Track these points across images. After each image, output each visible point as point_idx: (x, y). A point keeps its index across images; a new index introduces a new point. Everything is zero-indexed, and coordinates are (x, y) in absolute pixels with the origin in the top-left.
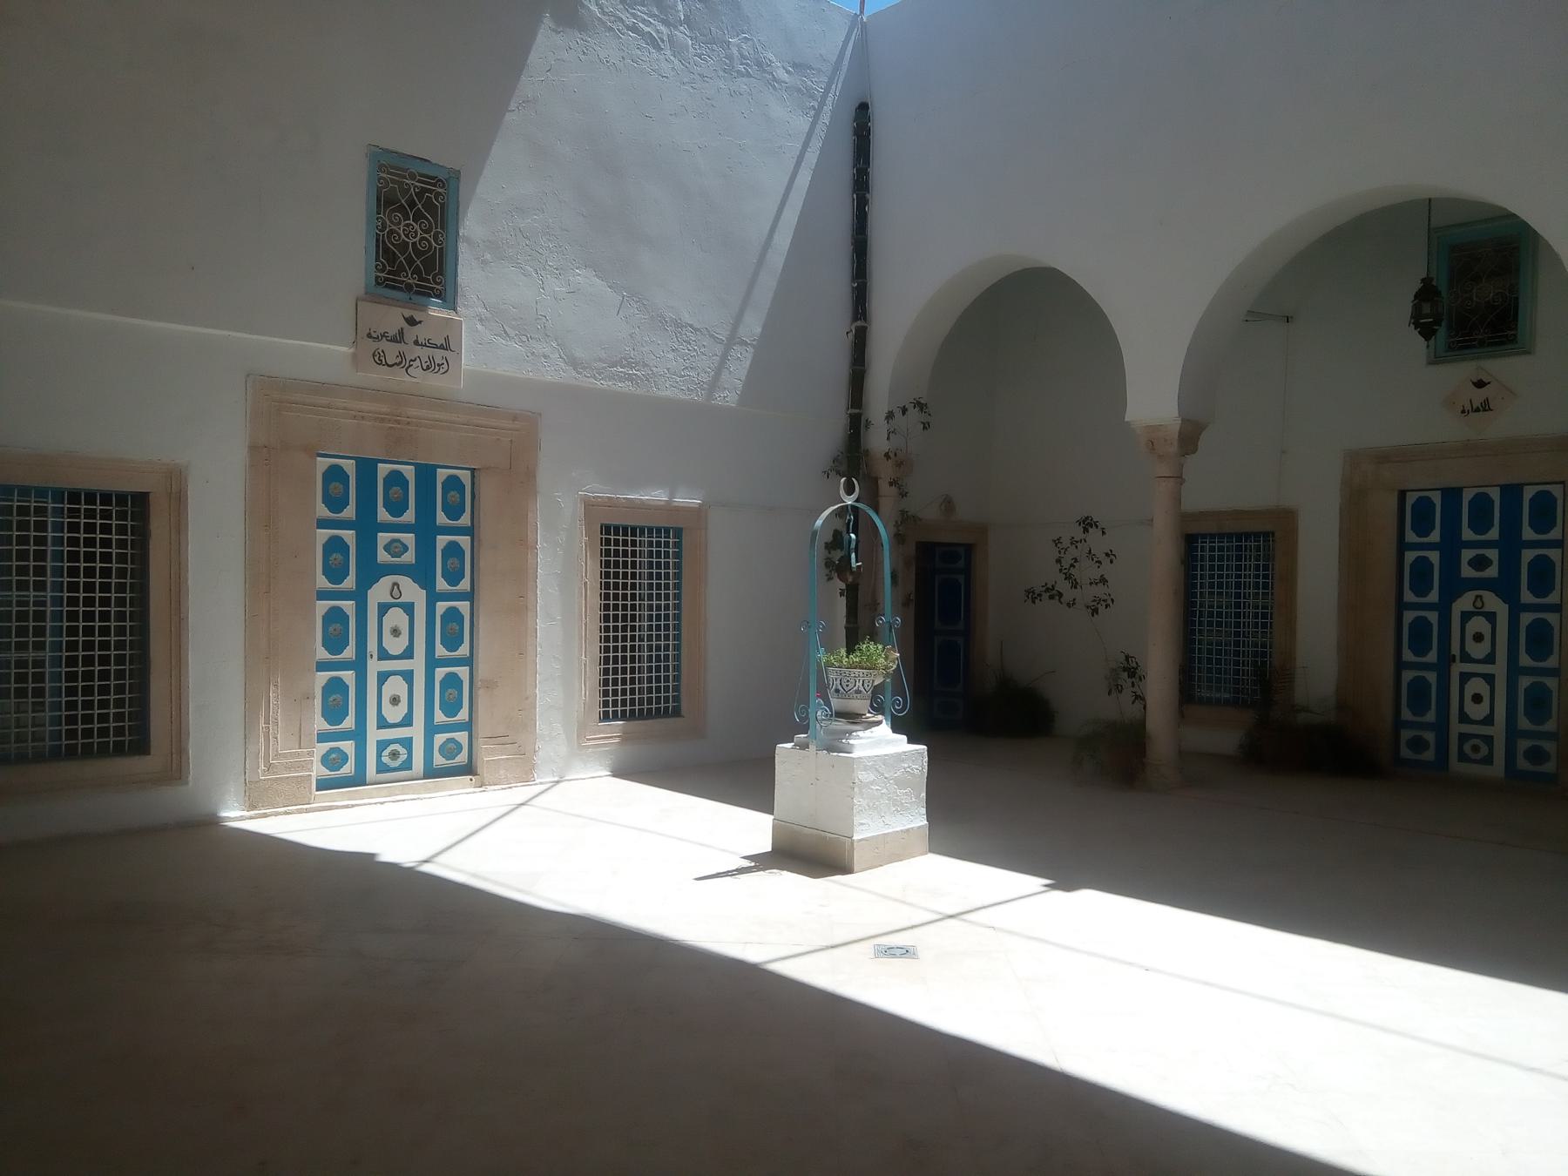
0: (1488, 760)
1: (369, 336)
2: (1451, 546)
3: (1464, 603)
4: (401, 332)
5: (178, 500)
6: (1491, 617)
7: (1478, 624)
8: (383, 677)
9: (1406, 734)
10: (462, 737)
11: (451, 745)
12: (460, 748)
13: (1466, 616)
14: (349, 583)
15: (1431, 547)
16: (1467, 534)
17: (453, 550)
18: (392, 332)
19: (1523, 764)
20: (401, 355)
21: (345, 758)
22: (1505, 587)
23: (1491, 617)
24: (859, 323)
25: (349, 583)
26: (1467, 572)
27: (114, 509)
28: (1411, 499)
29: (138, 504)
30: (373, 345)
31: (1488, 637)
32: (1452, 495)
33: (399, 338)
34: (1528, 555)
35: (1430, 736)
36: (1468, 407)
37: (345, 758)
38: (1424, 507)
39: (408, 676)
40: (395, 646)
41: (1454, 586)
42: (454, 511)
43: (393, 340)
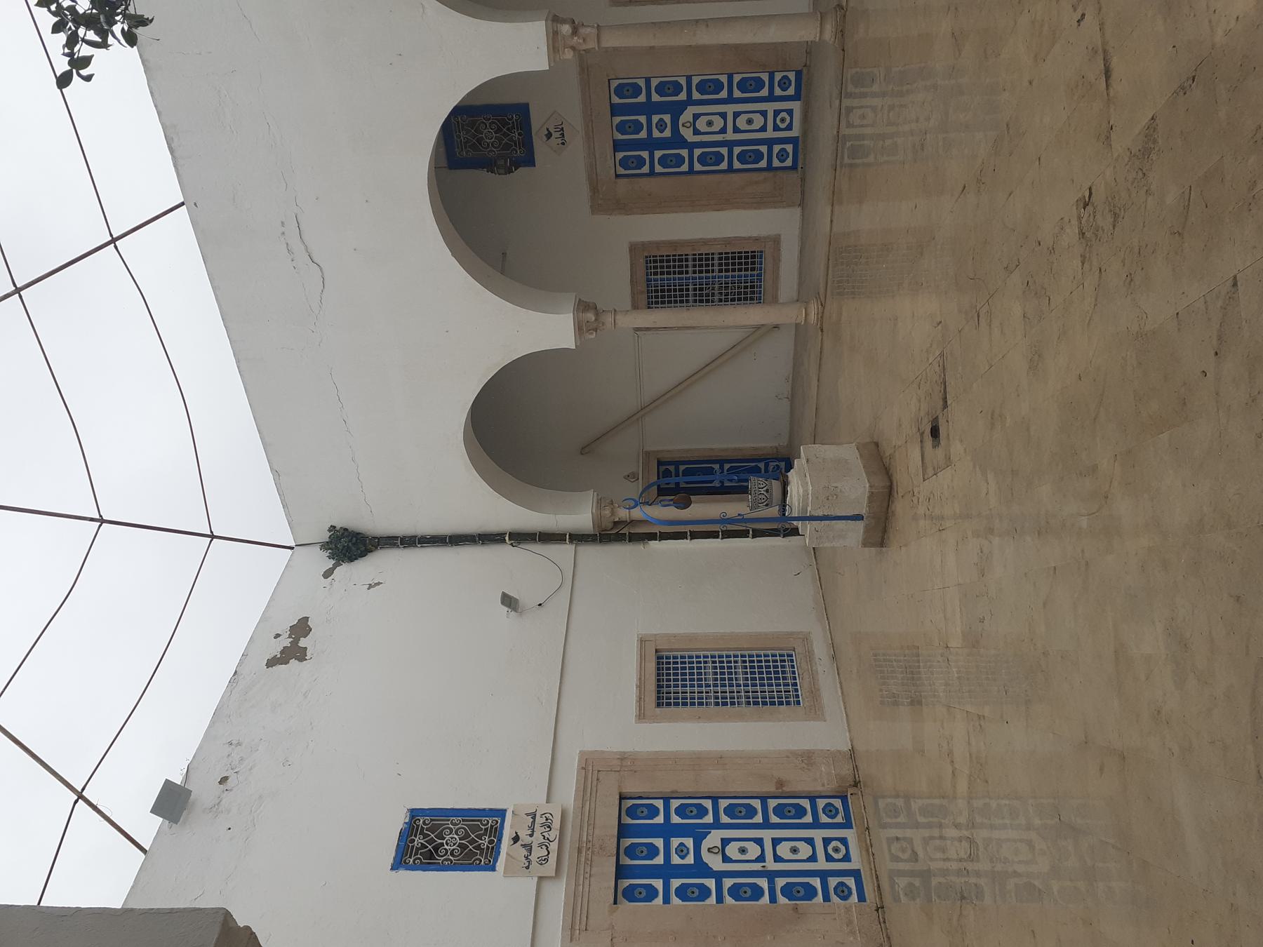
0: (790, 112)
1: (527, 868)
2: (651, 144)
4: (524, 846)
6: (696, 117)
7: (701, 125)
8: (777, 859)
9: (776, 163)
10: (821, 803)
11: (846, 892)
12: (829, 804)
13: (696, 132)
14: (711, 883)
15: (649, 95)
16: (643, 134)
18: (524, 852)
19: (791, 91)
20: (541, 845)
21: (782, 161)
22: (676, 110)
23: (696, 117)
25: (711, 883)
26: (667, 133)
27: (665, 690)
28: (621, 171)
29: (662, 700)
30: (534, 864)
31: (710, 118)
32: (617, 146)
33: (529, 847)
34: (656, 98)
35: (777, 148)
36: (560, 141)
37: (784, 90)
38: (624, 163)
41: (677, 141)
42: (636, 91)
43: (530, 851)
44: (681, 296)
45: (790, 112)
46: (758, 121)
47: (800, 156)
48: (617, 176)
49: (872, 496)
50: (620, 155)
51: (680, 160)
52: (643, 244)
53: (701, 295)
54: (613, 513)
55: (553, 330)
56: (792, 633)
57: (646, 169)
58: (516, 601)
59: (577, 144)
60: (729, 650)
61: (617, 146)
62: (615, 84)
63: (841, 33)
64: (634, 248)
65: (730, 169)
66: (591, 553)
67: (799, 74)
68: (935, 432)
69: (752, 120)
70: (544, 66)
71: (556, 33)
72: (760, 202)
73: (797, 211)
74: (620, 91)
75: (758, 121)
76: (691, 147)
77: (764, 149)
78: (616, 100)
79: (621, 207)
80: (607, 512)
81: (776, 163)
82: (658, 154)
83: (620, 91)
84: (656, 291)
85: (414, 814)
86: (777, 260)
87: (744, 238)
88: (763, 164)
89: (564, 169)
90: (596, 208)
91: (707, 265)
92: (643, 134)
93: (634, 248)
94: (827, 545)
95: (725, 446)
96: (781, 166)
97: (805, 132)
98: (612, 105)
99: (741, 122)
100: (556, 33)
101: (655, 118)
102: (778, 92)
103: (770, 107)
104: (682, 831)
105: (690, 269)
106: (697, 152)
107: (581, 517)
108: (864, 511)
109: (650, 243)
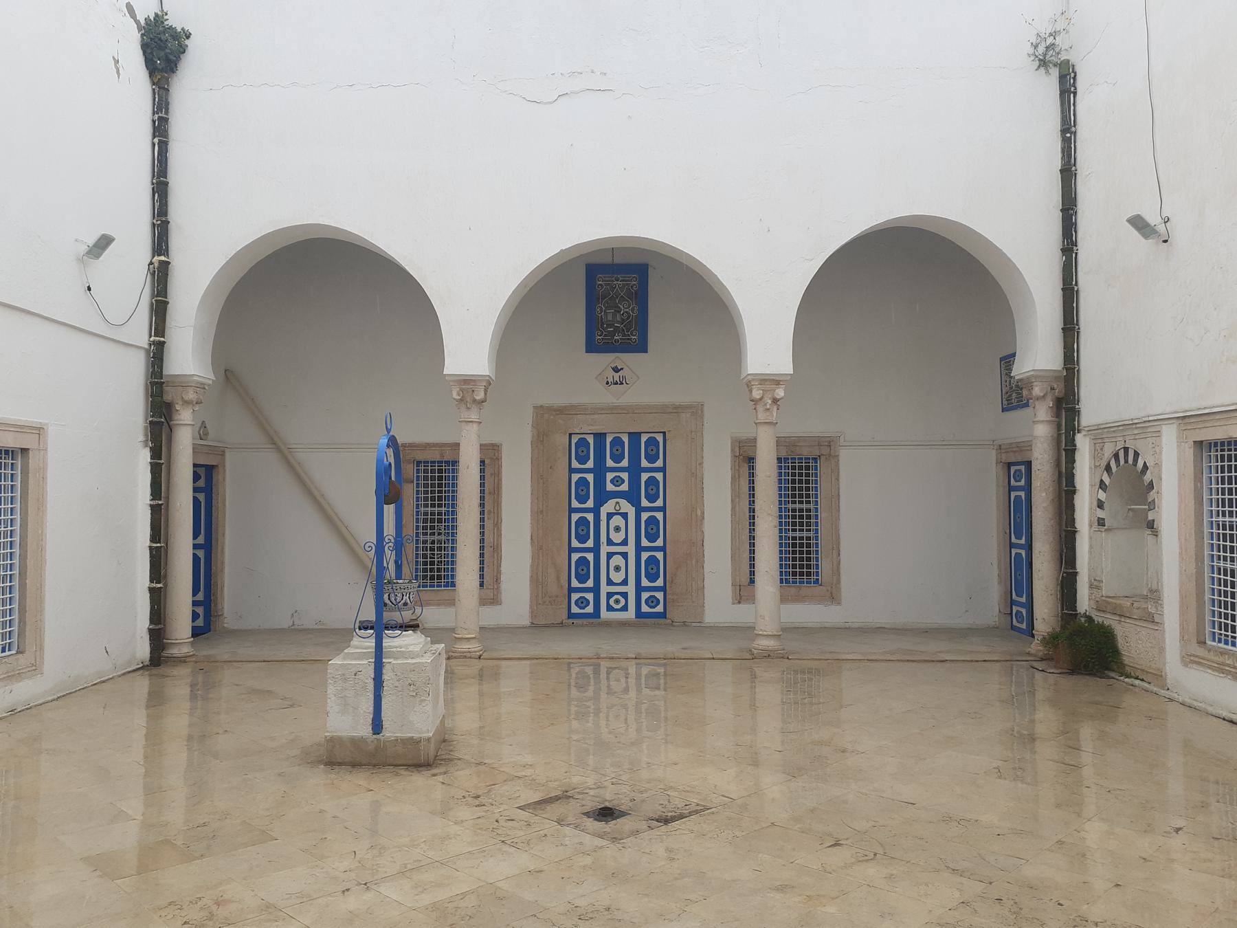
0: (625, 608)
2: (600, 471)
6: (625, 516)
7: (617, 521)
13: (610, 516)
15: (613, 470)
16: (610, 463)
17: (652, 482)
19: (645, 608)
21: (658, 602)
23: (625, 516)
24: (162, 258)
26: (610, 487)
28: (575, 440)
32: (600, 437)
34: (645, 476)
35: (590, 596)
36: (610, 380)
37: (658, 602)
38: (582, 443)
39: (625, 555)
40: (617, 537)
42: (652, 458)
44: (433, 499)
45: (625, 608)
46: (617, 577)
47: (585, 621)
48: (570, 435)
49: (414, 742)
50: (591, 440)
51: (582, 499)
52: (499, 459)
53: (432, 521)
54: (186, 403)
55: (768, 346)
56: (42, 649)
57: (575, 464)
58: (98, 256)
59: (608, 397)
61: (600, 437)
62: (660, 438)
63: (768, 655)
65: (571, 550)
66: (135, 369)
67: (663, 615)
68: (606, 813)
69: (619, 571)
70: (789, 369)
71: (778, 383)
72: (537, 581)
73: (525, 621)
74: (652, 442)
75: (617, 577)
76: (596, 511)
77: (590, 583)
78: (644, 438)
79: (541, 438)
80: (191, 395)
81: (575, 596)
82: (590, 477)
83: (652, 442)
84: (440, 471)
87: (499, 566)
88: (575, 584)
89: (584, 383)
90: (540, 411)
92: (610, 463)
94: (331, 690)
95: (227, 550)
96: (572, 602)
97: (608, 624)
99: (617, 560)
100: (778, 383)
101: (625, 476)
102: (645, 595)
103: (631, 589)
104: (634, 481)
106: (590, 517)
107: (188, 358)
108: (389, 732)
109: (500, 467)
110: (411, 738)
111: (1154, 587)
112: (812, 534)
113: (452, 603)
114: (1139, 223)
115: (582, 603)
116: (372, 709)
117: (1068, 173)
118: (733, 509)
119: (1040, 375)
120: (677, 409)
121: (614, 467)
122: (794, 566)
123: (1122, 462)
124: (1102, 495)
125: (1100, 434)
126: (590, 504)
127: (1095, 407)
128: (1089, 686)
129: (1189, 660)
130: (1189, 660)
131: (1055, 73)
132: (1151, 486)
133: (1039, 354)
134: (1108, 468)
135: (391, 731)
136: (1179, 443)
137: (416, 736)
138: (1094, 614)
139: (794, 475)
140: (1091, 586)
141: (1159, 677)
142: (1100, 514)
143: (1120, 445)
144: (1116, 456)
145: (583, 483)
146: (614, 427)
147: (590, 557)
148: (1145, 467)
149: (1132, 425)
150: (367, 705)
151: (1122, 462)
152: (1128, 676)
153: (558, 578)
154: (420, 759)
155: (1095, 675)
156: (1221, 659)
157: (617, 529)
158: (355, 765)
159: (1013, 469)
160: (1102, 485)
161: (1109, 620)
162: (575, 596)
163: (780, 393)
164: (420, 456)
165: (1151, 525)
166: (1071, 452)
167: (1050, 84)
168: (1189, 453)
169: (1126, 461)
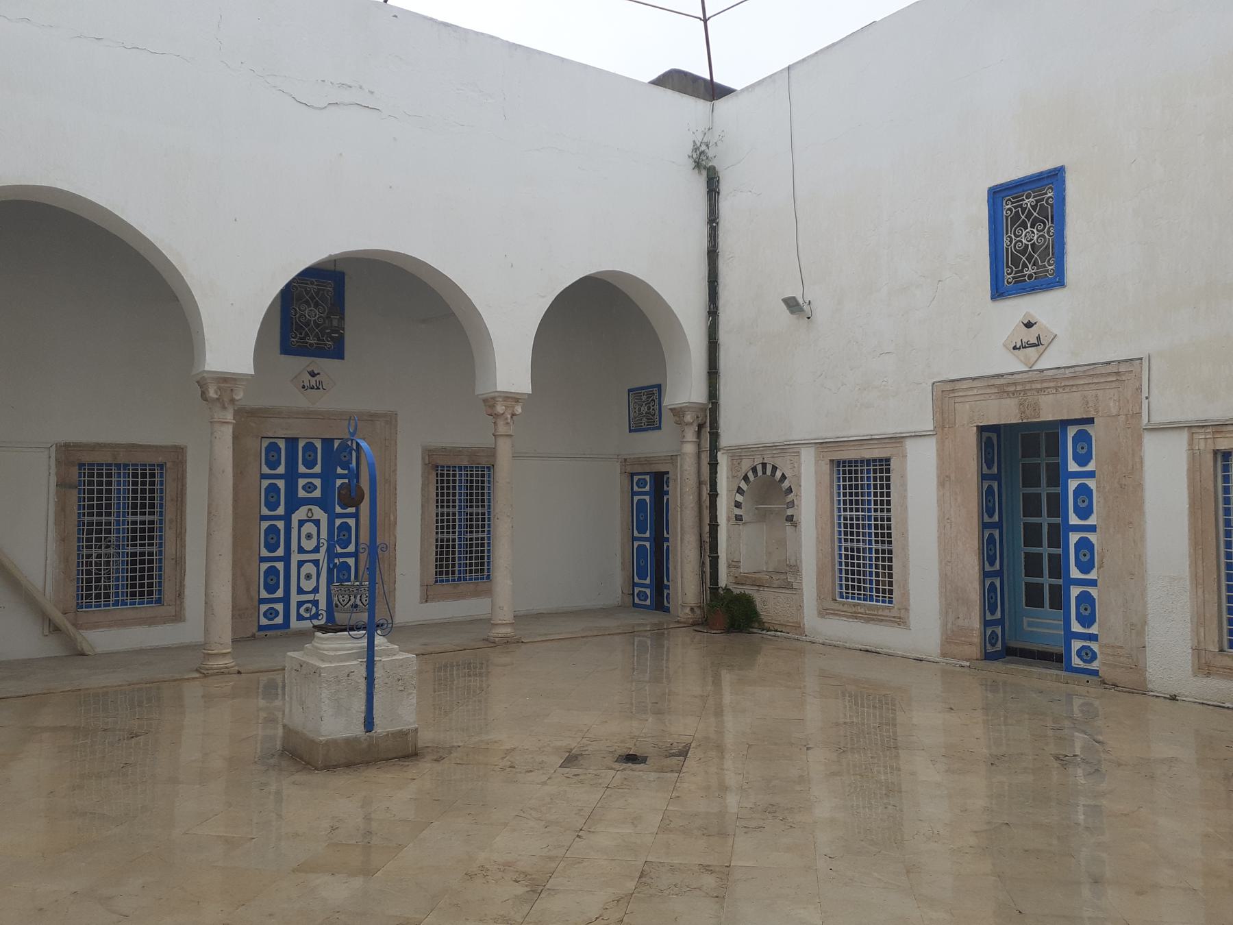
2: (291, 477)
3: (301, 513)
5: (67, 446)
6: (317, 523)
7: (309, 528)
11: (1083, 654)
13: (301, 523)
15: (645, 493)
16: (302, 469)
21: (277, 613)
23: (317, 523)
26: (302, 493)
32: (292, 442)
35: (279, 607)
36: (306, 384)
41: (294, 503)
50: (282, 444)
51: (272, 506)
59: (302, 401)
60: (833, 533)
64: (178, 453)
69: (309, 580)
71: (517, 401)
75: (308, 585)
76: (287, 518)
81: (264, 608)
85: (997, 194)
86: (151, 621)
89: (286, 390)
91: (142, 538)
92: (302, 469)
93: (178, 453)
98: (297, 439)
100: (517, 401)
101: (317, 482)
105: (451, 510)
106: (281, 524)
110: (401, 731)
111: (792, 562)
112: (154, 549)
113: (489, 592)
114: (792, 305)
115: (271, 614)
116: (363, 708)
117: (713, 254)
118: (423, 513)
119: (691, 407)
120: (372, 417)
121: (315, 473)
122: (134, 586)
123: (760, 473)
124: (739, 498)
125: (737, 453)
126: (281, 511)
127: (735, 430)
128: (739, 639)
129: (824, 613)
130: (824, 613)
131: (704, 173)
132: (790, 490)
133: (687, 389)
134: (746, 478)
135: (382, 726)
136: (817, 462)
137: (405, 728)
138: (731, 587)
139: (135, 483)
140: (729, 566)
141: (798, 627)
142: (738, 511)
143: (758, 461)
144: (754, 469)
145: (273, 489)
146: (304, 431)
147: (280, 566)
148: (784, 477)
149: (774, 447)
150: (359, 705)
151: (760, 473)
152: (769, 630)
153: (248, 590)
154: (404, 751)
155: (741, 631)
156: (854, 610)
157: (309, 536)
158: (349, 765)
159: (636, 478)
160: (740, 491)
161: (749, 590)
162: (264, 608)
163: (519, 410)
164: (87, 458)
165: (790, 519)
166: (714, 466)
167: (699, 185)
168: (826, 468)
169: (764, 473)
